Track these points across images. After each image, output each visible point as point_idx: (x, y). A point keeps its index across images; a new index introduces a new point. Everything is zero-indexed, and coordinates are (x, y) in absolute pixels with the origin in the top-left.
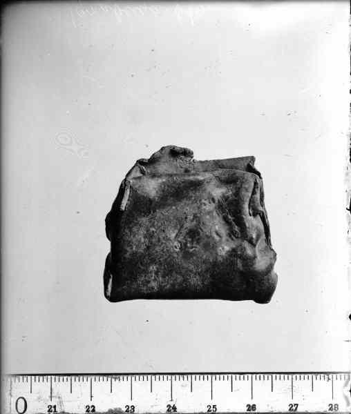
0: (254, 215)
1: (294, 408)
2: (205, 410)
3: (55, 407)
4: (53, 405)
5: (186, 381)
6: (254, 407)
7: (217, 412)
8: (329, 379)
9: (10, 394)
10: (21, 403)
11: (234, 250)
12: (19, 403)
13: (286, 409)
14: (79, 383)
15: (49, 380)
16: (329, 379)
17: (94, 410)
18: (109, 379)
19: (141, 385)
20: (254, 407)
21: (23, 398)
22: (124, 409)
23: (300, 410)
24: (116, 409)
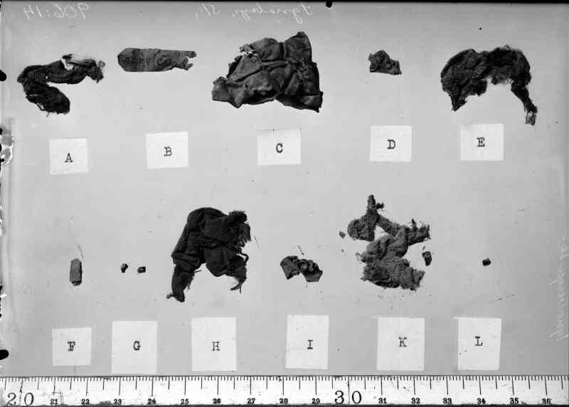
0: (261, 67)
1: (252, 401)
2: (79, 404)
3: (56, 400)
4: (55, 398)
5: (99, 383)
6: (219, 400)
7: (344, 403)
8: (280, 380)
9: (21, 391)
10: (29, 398)
11: (373, 237)
12: (359, 398)
13: (211, 402)
14: (14, 383)
15: (53, 380)
16: (280, 380)
17: (88, 403)
18: (86, 379)
19: (128, 385)
20: (219, 400)
21: (33, 397)
22: (113, 402)
23: (256, 402)
24: (106, 402)
